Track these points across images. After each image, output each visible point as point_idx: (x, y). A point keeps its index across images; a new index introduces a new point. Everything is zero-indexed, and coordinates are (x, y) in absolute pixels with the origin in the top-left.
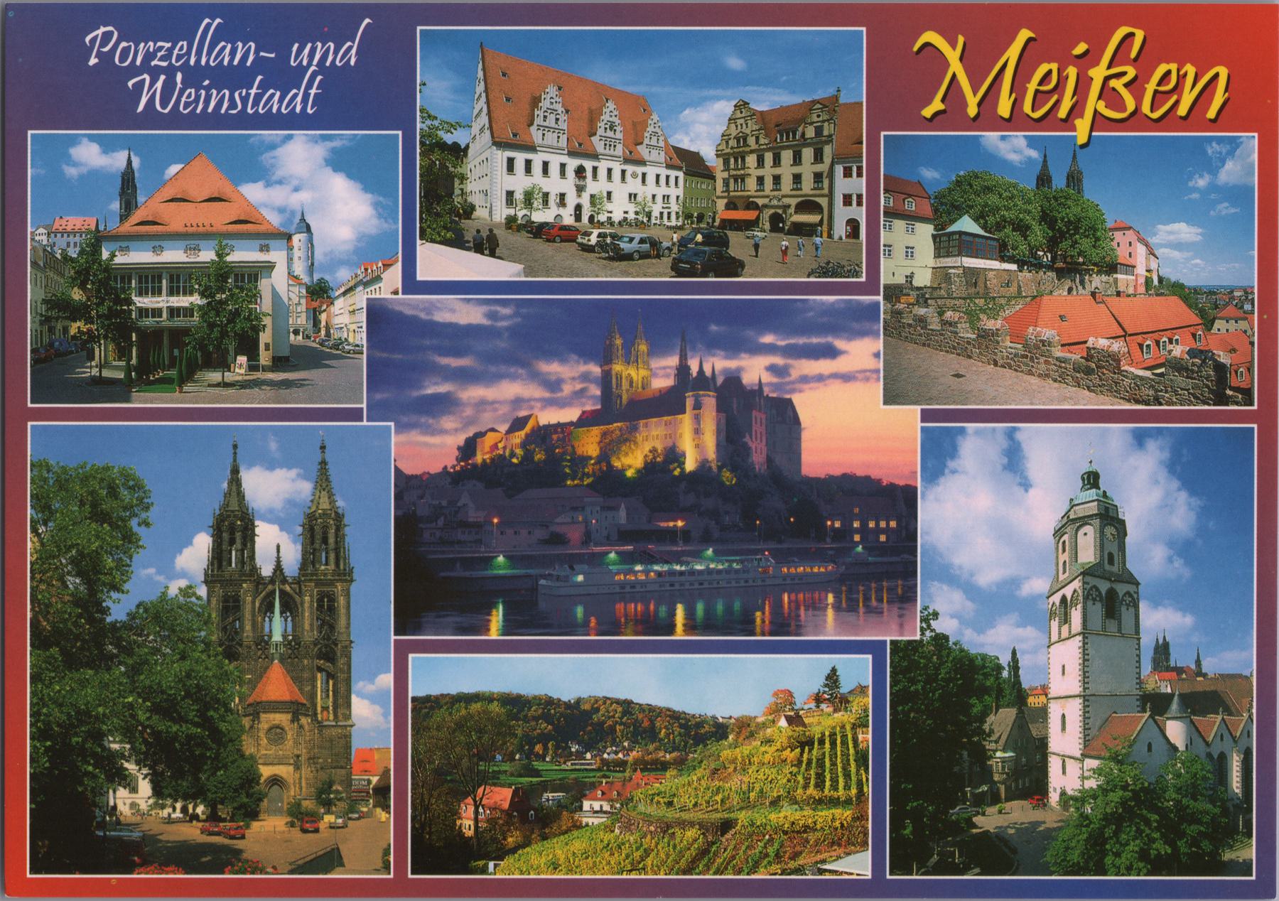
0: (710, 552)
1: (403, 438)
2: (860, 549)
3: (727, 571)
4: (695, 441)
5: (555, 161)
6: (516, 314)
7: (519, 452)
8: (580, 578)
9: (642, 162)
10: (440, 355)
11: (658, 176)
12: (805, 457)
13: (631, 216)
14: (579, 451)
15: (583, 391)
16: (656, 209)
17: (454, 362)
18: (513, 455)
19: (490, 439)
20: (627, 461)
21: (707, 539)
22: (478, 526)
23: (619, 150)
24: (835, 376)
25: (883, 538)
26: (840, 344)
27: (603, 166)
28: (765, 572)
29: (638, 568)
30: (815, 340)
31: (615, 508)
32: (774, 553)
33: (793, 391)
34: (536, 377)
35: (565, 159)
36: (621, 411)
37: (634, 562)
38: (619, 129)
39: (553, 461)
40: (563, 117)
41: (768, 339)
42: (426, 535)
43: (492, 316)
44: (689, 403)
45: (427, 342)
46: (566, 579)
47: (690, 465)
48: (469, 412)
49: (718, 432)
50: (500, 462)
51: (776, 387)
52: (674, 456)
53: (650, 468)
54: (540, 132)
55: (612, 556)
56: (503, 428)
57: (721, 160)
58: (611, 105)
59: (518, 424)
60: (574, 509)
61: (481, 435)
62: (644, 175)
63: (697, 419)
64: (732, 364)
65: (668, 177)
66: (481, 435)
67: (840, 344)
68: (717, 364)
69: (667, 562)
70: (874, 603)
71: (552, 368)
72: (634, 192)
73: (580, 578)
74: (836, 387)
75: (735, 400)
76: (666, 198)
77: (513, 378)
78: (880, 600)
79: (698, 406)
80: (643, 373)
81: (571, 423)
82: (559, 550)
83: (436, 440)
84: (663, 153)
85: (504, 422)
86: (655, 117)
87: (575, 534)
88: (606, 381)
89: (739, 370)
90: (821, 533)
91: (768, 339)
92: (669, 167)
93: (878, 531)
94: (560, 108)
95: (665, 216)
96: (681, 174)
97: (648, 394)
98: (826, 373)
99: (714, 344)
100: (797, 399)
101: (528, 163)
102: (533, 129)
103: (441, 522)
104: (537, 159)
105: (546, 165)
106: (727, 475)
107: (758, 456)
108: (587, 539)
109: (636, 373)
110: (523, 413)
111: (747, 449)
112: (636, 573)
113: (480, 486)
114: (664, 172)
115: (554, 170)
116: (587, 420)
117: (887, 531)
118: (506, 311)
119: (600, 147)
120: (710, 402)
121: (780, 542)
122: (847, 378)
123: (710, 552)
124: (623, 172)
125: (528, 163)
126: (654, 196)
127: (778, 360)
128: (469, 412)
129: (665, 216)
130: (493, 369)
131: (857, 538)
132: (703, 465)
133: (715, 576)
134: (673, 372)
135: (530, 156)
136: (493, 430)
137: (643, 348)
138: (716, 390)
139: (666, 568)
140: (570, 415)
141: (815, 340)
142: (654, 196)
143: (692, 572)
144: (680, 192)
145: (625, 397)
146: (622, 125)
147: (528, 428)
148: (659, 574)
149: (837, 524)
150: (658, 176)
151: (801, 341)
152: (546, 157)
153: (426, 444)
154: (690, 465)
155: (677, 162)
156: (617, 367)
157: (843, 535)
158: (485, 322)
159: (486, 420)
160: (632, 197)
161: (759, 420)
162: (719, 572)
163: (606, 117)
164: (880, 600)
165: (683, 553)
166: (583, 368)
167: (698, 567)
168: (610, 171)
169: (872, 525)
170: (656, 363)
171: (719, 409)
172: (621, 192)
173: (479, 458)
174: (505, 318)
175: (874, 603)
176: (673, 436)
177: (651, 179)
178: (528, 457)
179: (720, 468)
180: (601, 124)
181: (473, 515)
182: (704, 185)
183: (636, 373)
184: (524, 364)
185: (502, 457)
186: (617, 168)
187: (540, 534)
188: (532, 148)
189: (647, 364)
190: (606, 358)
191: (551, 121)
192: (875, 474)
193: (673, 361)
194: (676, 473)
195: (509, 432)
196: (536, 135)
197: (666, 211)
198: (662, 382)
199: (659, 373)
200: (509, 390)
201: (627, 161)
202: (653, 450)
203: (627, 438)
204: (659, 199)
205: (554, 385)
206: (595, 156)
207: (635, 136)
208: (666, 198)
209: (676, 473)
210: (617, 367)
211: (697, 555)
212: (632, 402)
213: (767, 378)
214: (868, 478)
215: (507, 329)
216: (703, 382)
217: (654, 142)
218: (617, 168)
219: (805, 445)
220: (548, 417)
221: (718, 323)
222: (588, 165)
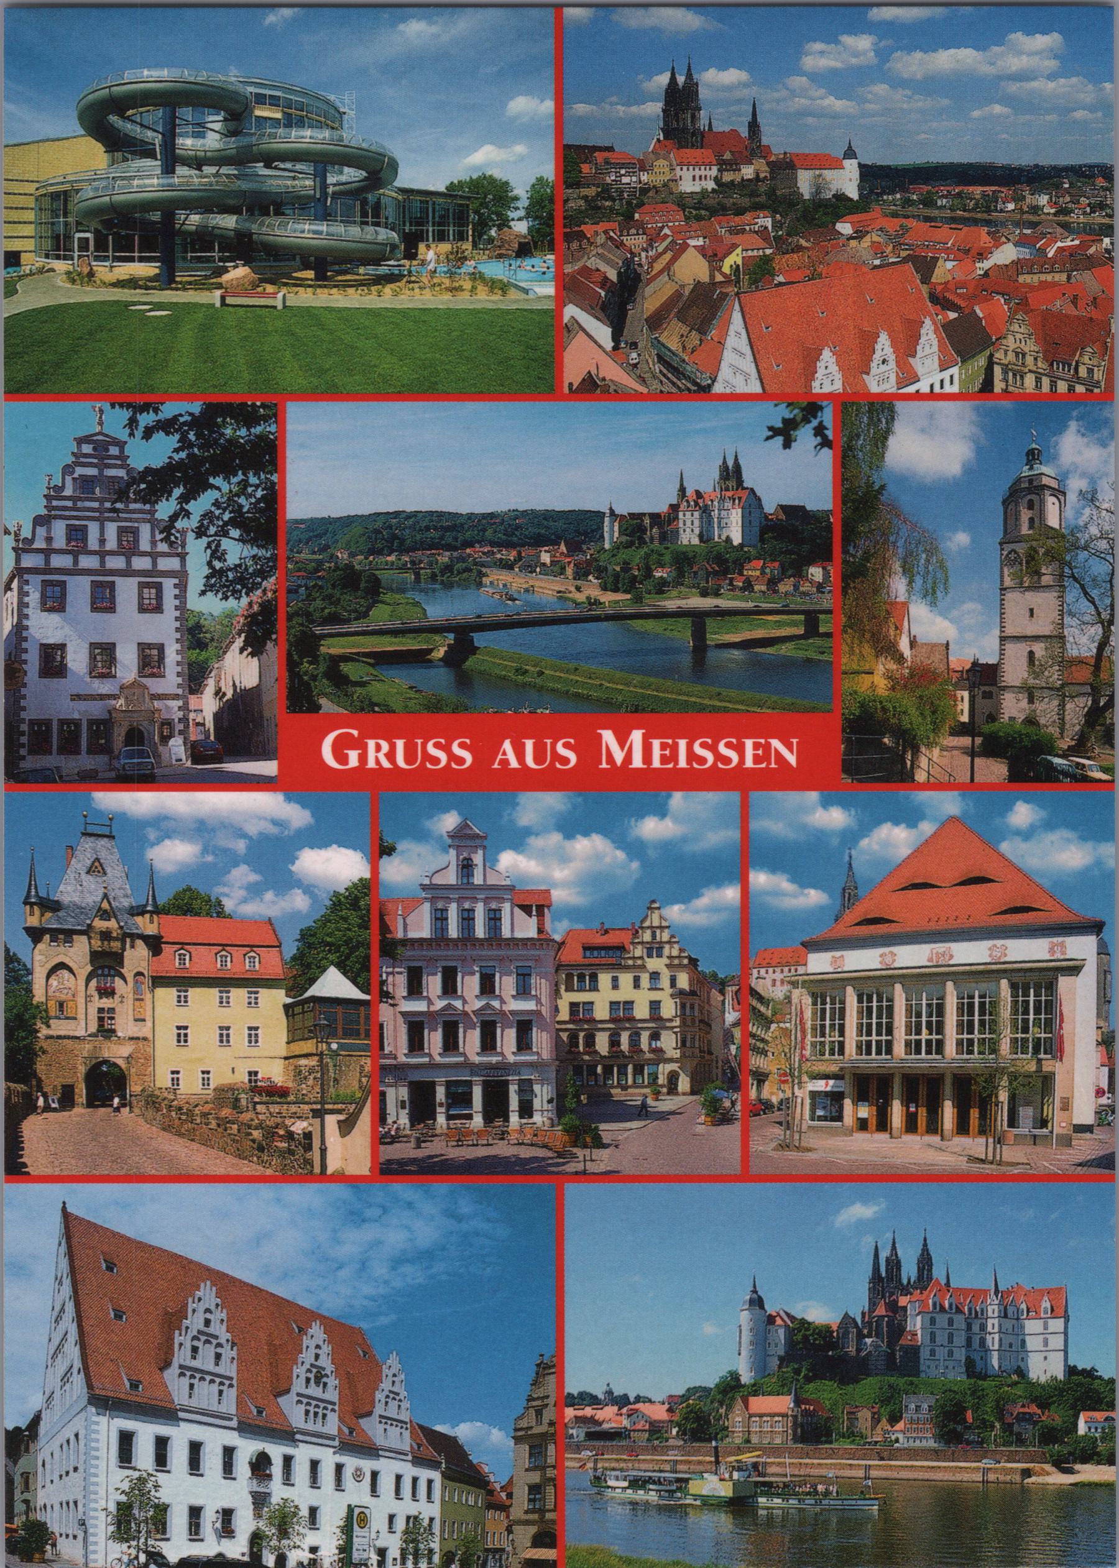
9: (370, 1450)
11: (399, 1478)
23: (333, 1425)
35: (232, 1438)
38: (332, 1382)
40: (228, 1353)
54: (185, 1381)
62: (375, 1475)
65: (415, 1480)
86: (393, 1364)
94: (224, 1336)
96: (436, 1476)
101: (162, 1443)
104: (180, 1436)
105: (195, 1448)
114: (408, 1470)
115: (212, 1460)
124: (339, 1468)
126: (391, 1517)
142: (391, 1517)
146: (337, 1373)
150: (399, 1478)
155: (430, 1452)
163: (307, 1357)
168: (314, 1465)
177: (386, 1484)
180: (300, 1371)
186: (328, 1458)
188: (168, 1413)
191: (207, 1354)
206: (288, 1435)
217: (392, 1412)
222: (276, 1452)
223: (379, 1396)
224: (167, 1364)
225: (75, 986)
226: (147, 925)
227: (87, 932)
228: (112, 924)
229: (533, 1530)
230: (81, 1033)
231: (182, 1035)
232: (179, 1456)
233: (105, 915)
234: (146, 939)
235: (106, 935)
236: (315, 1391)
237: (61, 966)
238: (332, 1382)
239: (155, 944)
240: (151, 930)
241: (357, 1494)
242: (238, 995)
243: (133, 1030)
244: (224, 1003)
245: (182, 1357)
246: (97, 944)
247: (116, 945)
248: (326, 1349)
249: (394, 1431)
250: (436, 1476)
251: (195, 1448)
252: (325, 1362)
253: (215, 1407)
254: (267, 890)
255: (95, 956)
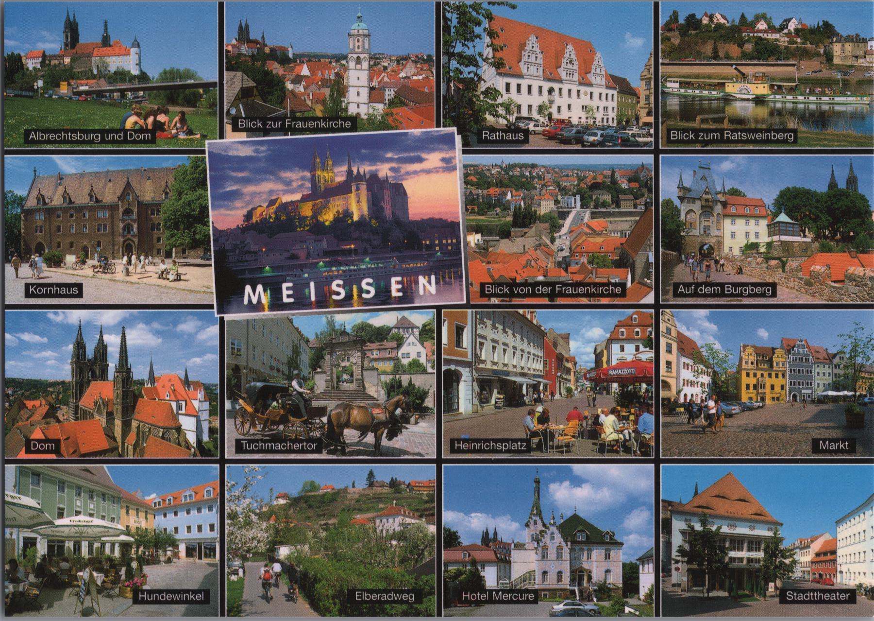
0: (368, 259)
1: (216, 212)
2: (439, 254)
3: (377, 268)
4: (357, 206)
5: (535, 85)
6: (268, 150)
7: (273, 216)
8: (306, 275)
9: (590, 85)
10: (233, 171)
11: (600, 94)
12: (411, 211)
13: (583, 120)
14: (302, 214)
15: (302, 185)
16: (599, 116)
17: (240, 175)
18: (270, 217)
19: (259, 211)
20: (325, 217)
21: (366, 253)
22: (256, 253)
23: (576, 77)
24: (423, 171)
25: (450, 248)
26: (424, 156)
27: (565, 88)
28: (395, 266)
29: (334, 269)
30: (412, 154)
31: (321, 241)
32: (398, 258)
33: (403, 179)
34: (279, 179)
35: (542, 83)
36: (321, 194)
37: (331, 266)
38: (576, 63)
39: (290, 220)
40: (540, 56)
41: (389, 155)
42: (231, 258)
43: (256, 151)
44: (354, 188)
45: (226, 166)
46: (300, 276)
47: (356, 218)
48: (248, 198)
49: (368, 200)
50: (264, 221)
51: (394, 178)
52: (348, 214)
53: (337, 220)
54: (526, 66)
55: (321, 263)
56: (265, 205)
57: (644, 82)
58: (570, 47)
59: (272, 203)
60: (302, 242)
61: (255, 209)
62: (591, 93)
63: (358, 195)
64: (373, 168)
66: (255, 209)
67: (424, 156)
68: (366, 168)
69: (347, 265)
70: (447, 279)
71: (287, 175)
72: (585, 104)
73: (306, 275)
74: (423, 178)
75: (374, 183)
76: (606, 108)
77: (269, 180)
78: (450, 278)
79: (358, 189)
80: (330, 174)
81: (298, 201)
82: (293, 262)
83: (232, 213)
84: (604, 79)
85: (265, 202)
86: (599, 55)
87: (302, 254)
88: (313, 180)
89: (377, 170)
90: (420, 247)
91: (389, 155)
92: (608, 87)
93: (447, 245)
94: (538, 51)
95: (605, 120)
96: (615, 92)
97: (334, 185)
98: (418, 170)
99: (363, 159)
100: (406, 184)
101: (519, 86)
102: (521, 64)
103: (237, 252)
104: (524, 83)
105: (530, 87)
106: (373, 221)
107: (388, 212)
108: (308, 255)
109: (327, 175)
110: (274, 197)
111: (382, 208)
112: (333, 272)
113: (255, 233)
114: (604, 91)
115: (535, 90)
116: (305, 199)
117: (452, 244)
118: (263, 148)
119: (563, 76)
120: (363, 187)
121: (400, 252)
122: (428, 172)
123: (368, 259)
124: (579, 91)
125: (519, 86)
127: (394, 165)
128: (248, 198)
129: (605, 120)
130: (258, 177)
131: (437, 248)
132: (362, 217)
133: (371, 271)
134: (345, 174)
135: (519, 81)
136: (260, 206)
137: (330, 163)
138: (366, 181)
139: (347, 268)
140: (297, 197)
141: (412, 154)
143: (360, 270)
144: (615, 104)
145: (322, 187)
146: (578, 61)
147: (277, 205)
148: (344, 271)
149: (428, 243)
151: (405, 155)
152: (530, 82)
153: (229, 215)
154: (356, 218)
155: (612, 83)
156: (319, 173)
157: (430, 247)
158: (254, 154)
159: (257, 202)
160: (584, 107)
161: (387, 195)
162: (373, 269)
163: (567, 56)
164: (450, 278)
165: (355, 261)
166: (301, 174)
167: (363, 267)
168: (570, 91)
169: (444, 242)
170: (336, 170)
171: (368, 190)
172: (577, 104)
173: (254, 220)
174: (263, 152)
175: (447, 279)
176: (348, 204)
177: (596, 96)
178: (277, 218)
179: (370, 219)
180: (564, 61)
181: (254, 248)
182: (630, 100)
183: (327, 175)
184: (272, 173)
185: (265, 219)
186: (574, 89)
187: (286, 255)
188: (520, 76)
189: (332, 170)
190: (313, 169)
191: (532, 59)
192: (444, 217)
193: (345, 168)
194: (349, 222)
195: (268, 206)
196: (523, 68)
197: (605, 117)
198: (340, 179)
199: (338, 174)
200: (267, 186)
201: (581, 84)
202: (338, 212)
203: (325, 206)
204: (601, 109)
205: (288, 183)
206: (560, 81)
207: (585, 69)
208: (606, 108)
209: (349, 222)
210: (319, 173)
211: (362, 261)
212: (326, 189)
213: (390, 174)
214: (441, 219)
215: (265, 157)
216: (360, 178)
217: (598, 71)
218: (574, 89)
219: (410, 205)
220: (286, 199)
221: (365, 148)
222: (556, 86)
223: (593, 67)
224: (521, 61)
225: (694, 217)
226: (721, 198)
227: (700, 199)
228: (709, 196)
229: (647, 110)
230: (698, 234)
231: (733, 235)
232: (524, 89)
233: (706, 193)
234: (721, 202)
235: (707, 200)
236: (569, 66)
237: (691, 211)
238: (576, 63)
239: (725, 205)
240: (723, 199)
241: (585, 100)
242: (752, 222)
243: (716, 233)
244: (747, 224)
245: (525, 59)
246: (703, 203)
247: (711, 204)
248: (573, 52)
249: (598, 78)
250: (615, 92)
251: (530, 87)
252: (574, 57)
253: (535, 74)
254: (679, 44)
255: (702, 207)
